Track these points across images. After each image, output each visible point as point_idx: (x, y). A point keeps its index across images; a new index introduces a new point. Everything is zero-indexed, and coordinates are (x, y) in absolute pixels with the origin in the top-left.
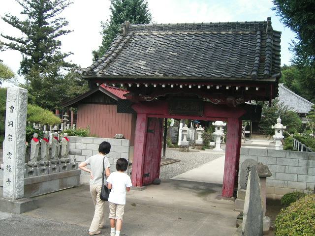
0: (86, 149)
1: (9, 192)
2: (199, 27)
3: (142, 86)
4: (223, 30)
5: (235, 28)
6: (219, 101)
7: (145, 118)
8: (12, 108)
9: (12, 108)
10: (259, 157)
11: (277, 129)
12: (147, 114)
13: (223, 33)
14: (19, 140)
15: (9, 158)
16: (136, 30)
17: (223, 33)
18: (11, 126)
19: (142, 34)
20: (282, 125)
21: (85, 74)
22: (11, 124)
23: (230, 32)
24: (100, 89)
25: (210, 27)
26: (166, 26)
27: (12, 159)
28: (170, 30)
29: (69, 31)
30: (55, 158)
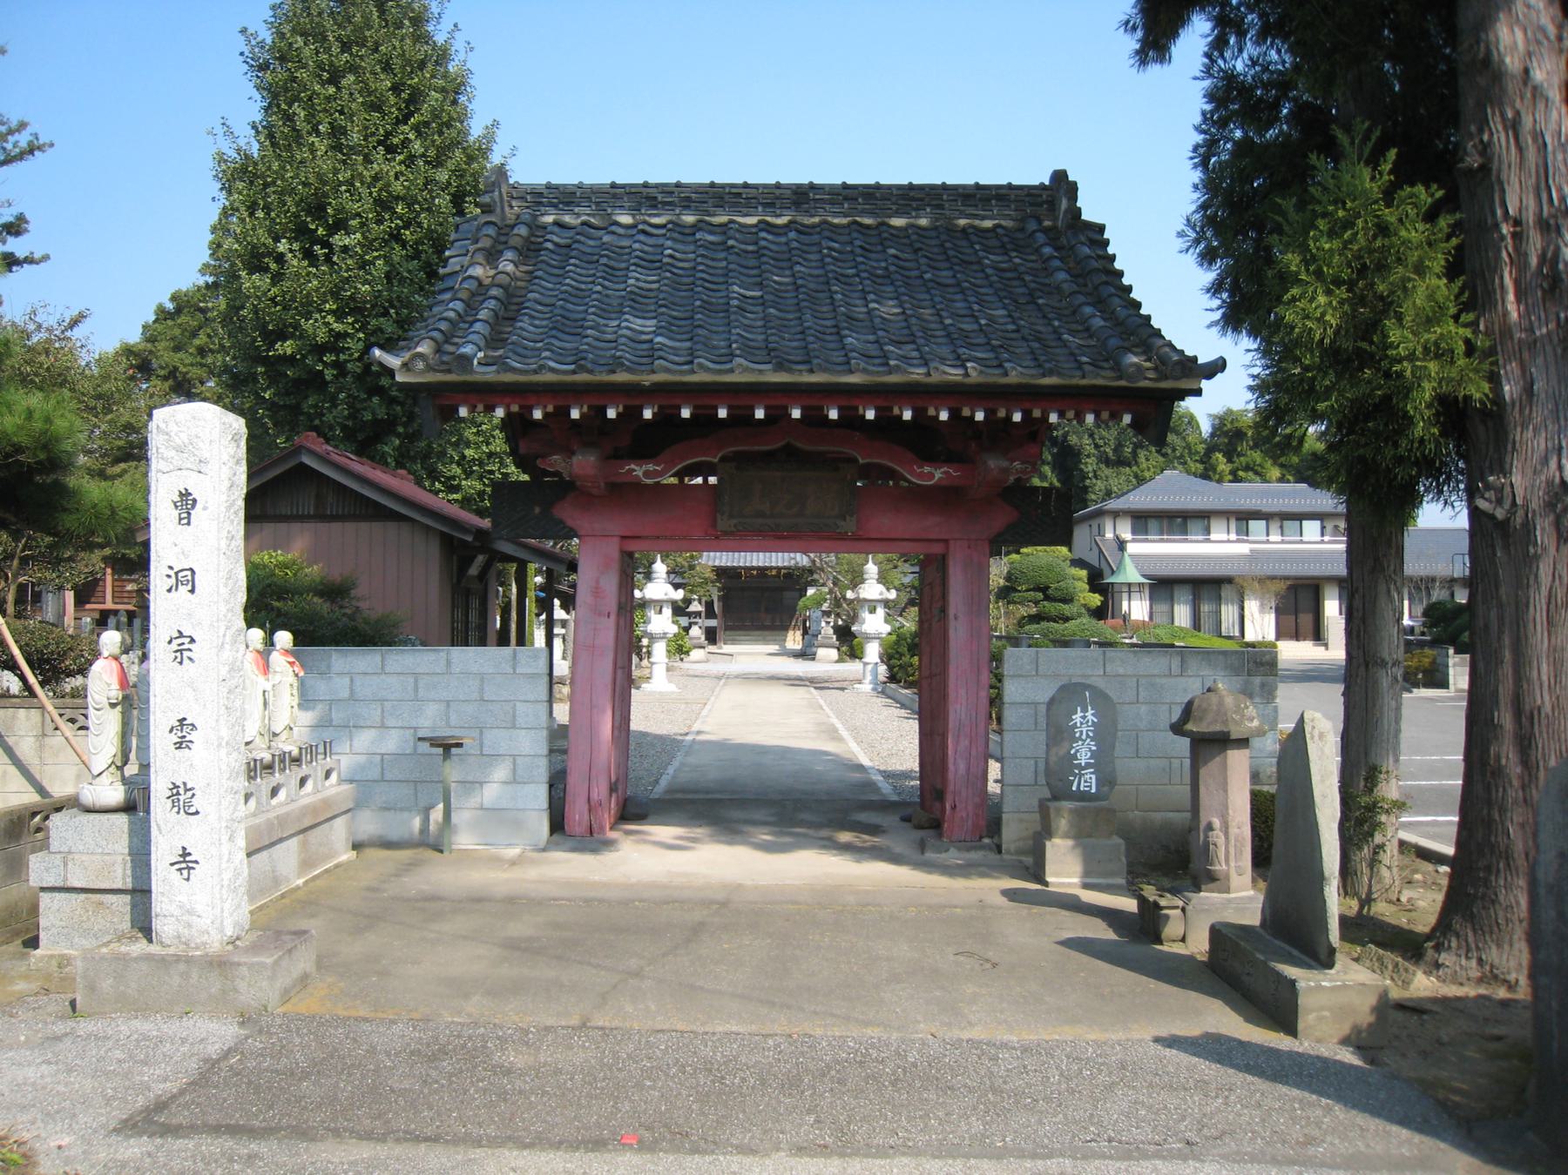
0: (353, 697)
1: (191, 912)
2: (802, 196)
3: (631, 414)
4: (898, 214)
5: (940, 207)
6: (938, 475)
7: (616, 555)
8: (186, 502)
9: (186, 502)
10: (518, 704)
11: (866, 600)
12: (623, 538)
13: (898, 222)
14: (227, 654)
15: (178, 746)
16: (540, 203)
17: (898, 222)
18: (183, 589)
19: (567, 219)
20: (881, 588)
21: (420, 365)
22: (186, 579)
23: (923, 222)
24: (307, 460)
25: (846, 199)
26: (664, 188)
27: (200, 749)
28: (687, 207)
29: (30, 260)
30: (258, 740)
